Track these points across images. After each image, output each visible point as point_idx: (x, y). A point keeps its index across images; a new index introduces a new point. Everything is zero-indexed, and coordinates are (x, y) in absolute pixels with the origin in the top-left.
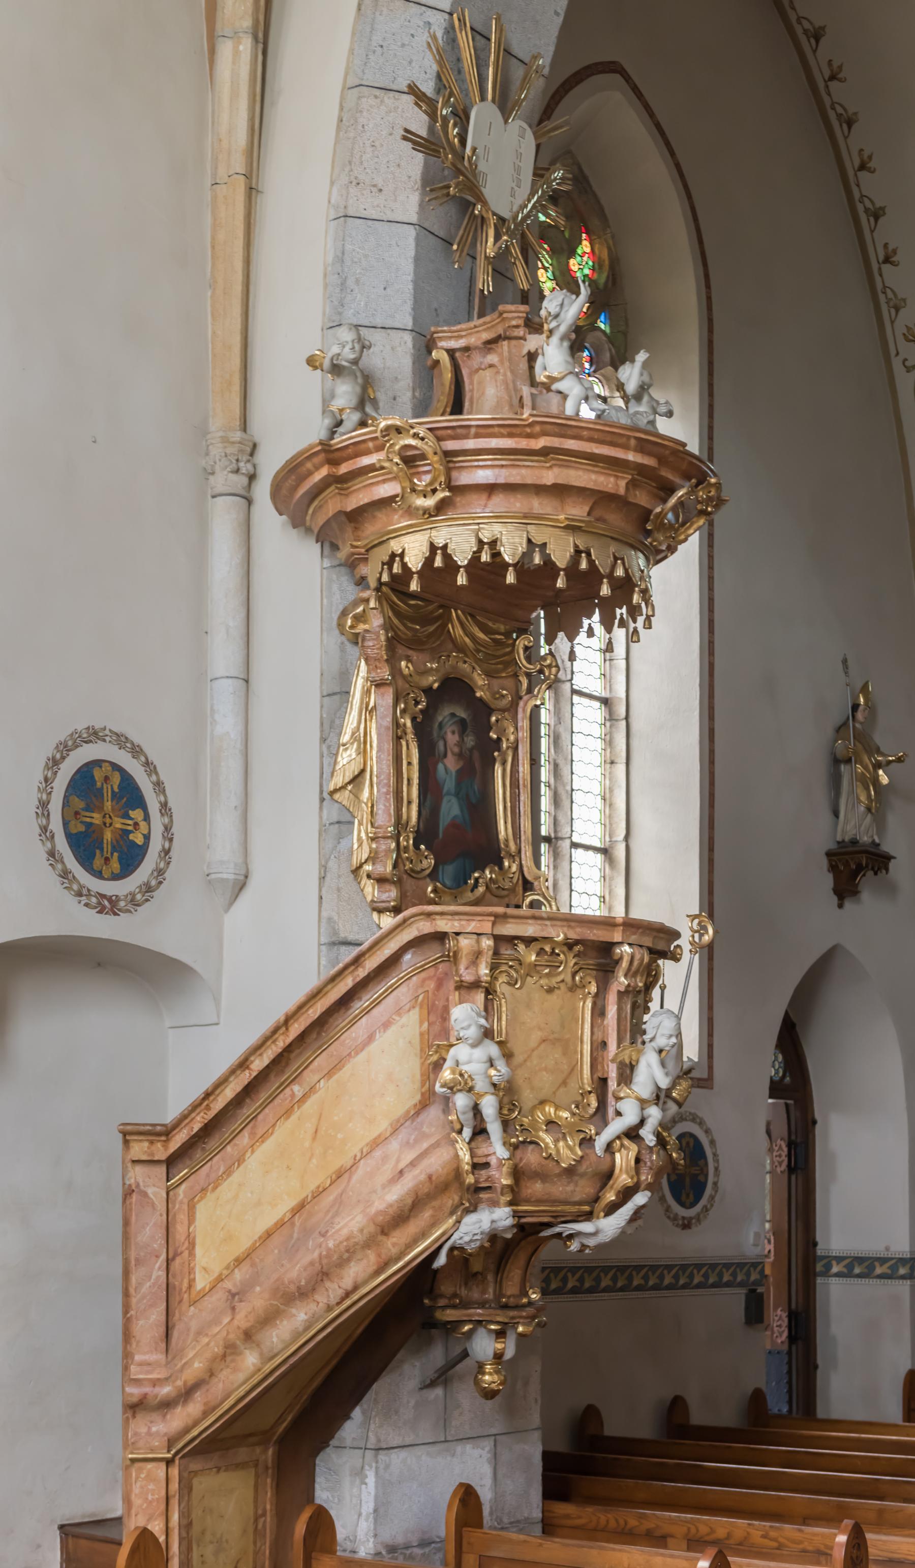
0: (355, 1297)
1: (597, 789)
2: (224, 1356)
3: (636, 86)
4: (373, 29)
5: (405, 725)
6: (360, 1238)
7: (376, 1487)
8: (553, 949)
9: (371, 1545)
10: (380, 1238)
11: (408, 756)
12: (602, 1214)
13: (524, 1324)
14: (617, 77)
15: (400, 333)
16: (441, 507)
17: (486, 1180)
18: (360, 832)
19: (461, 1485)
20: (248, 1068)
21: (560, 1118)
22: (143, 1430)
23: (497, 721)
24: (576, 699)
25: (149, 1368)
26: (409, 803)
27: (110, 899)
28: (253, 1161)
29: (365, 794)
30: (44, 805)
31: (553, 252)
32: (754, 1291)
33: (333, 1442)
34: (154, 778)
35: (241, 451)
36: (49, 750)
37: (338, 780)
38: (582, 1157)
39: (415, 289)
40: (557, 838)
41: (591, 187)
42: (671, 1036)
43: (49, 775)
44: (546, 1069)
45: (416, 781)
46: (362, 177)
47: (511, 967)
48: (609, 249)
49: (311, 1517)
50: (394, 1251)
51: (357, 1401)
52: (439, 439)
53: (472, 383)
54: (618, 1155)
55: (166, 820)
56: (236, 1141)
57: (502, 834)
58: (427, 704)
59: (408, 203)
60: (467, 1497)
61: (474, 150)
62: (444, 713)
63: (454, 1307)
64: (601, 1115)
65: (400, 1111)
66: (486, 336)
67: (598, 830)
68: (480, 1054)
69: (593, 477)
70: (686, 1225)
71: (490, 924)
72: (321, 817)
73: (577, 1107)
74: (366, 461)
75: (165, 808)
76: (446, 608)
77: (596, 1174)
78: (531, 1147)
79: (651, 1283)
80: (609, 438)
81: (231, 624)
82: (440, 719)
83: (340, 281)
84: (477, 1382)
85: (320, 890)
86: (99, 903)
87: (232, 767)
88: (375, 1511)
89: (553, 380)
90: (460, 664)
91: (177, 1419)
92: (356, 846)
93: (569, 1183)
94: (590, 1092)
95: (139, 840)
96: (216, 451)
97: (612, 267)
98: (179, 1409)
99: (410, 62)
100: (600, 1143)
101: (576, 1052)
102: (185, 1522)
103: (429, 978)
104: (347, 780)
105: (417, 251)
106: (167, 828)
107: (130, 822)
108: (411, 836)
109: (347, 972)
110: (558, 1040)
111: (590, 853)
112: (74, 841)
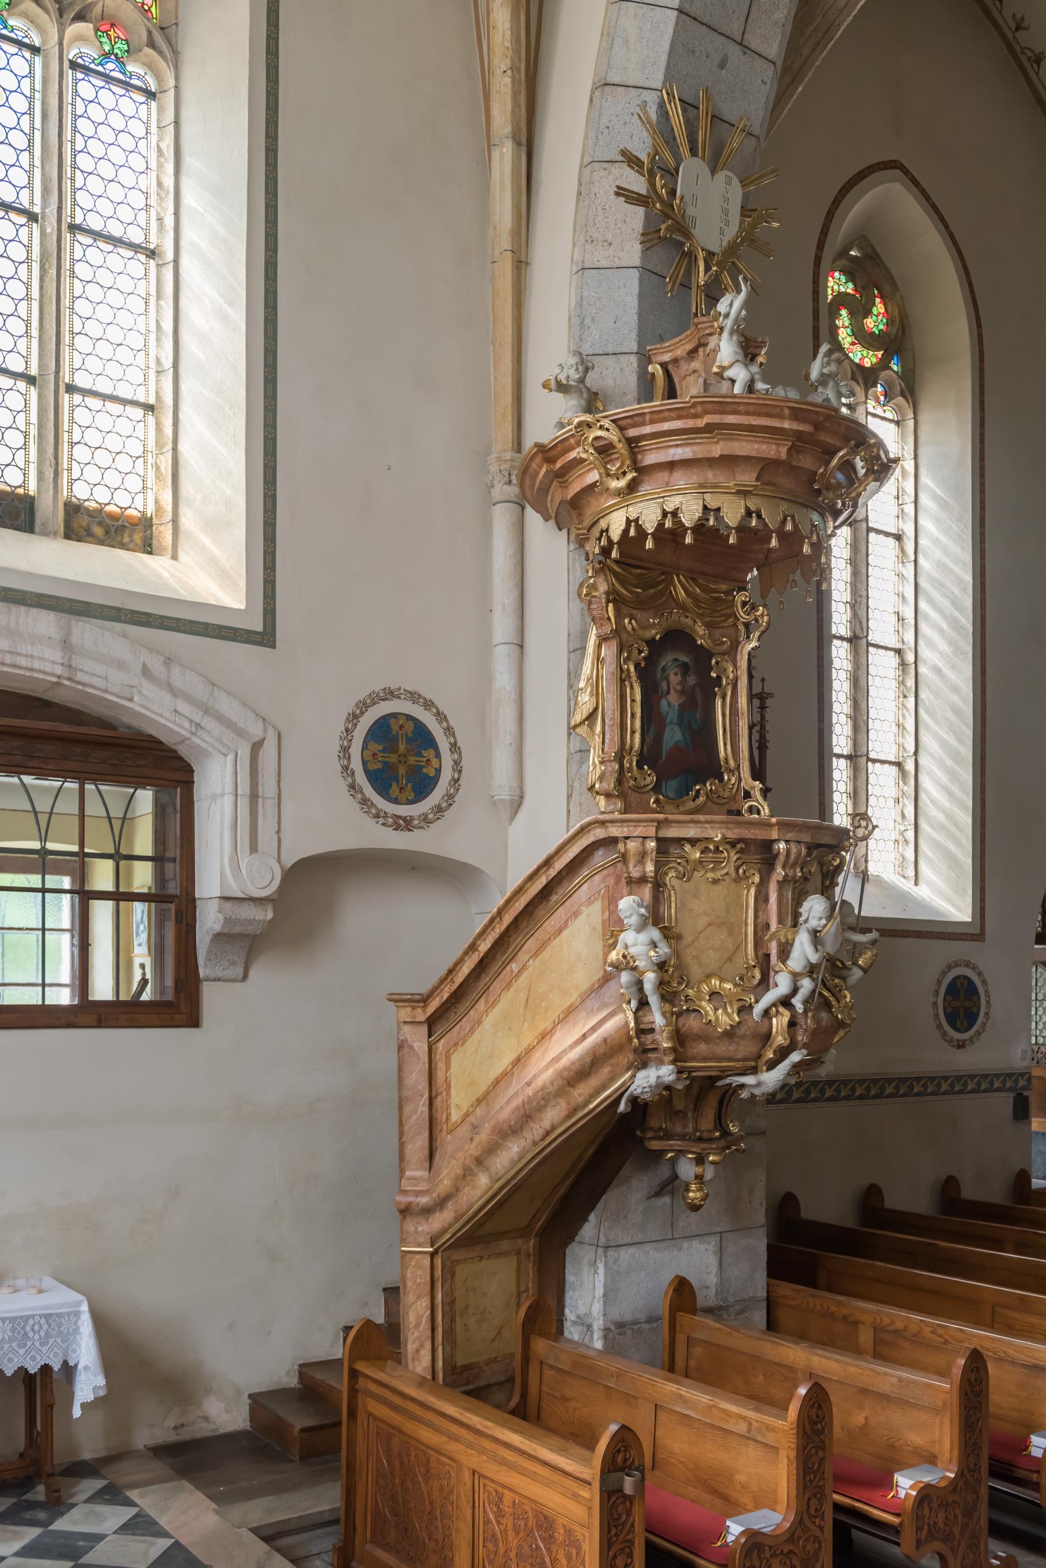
0: (553, 1136)
1: (892, 718)
2: (464, 1177)
3: (913, 177)
4: (600, 114)
5: (628, 670)
6: (552, 1089)
7: (605, 1277)
8: (717, 848)
9: (601, 1322)
10: (568, 1089)
11: (632, 694)
12: (765, 1068)
13: (714, 1154)
14: (897, 173)
15: (628, 357)
16: (632, 487)
17: (652, 1043)
18: (594, 757)
19: (677, 1276)
20: (476, 950)
21: (724, 989)
22: (412, 1229)
23: (717, 663)
24: (871, 649)
25: (415, 1182)
26: (633, 732)
27: (404, 819)
28: (488, 1022)
29: (598, 728)
30: (345, 750)
31: (851, 314)
32: (1021, 1094)
33: (577, 1238)
34: (445, 724)
35: (513, 467)
36: (350, 707)
37: (578, 718)
38: (739, 1023)
39: (639, 319)
40: (856, 756)
41: (882, 261)
42: (820, 919)
43: (350, 726)
44: (712, 948)
45: (639, 715)
46: (595, 235)
47: (679, 864)
48: (899, 307)
49: (529, 1307)
50: (580, 1100)
51: (592, 1208)
52: (622, 429)
53: (681, 389)
54: (774, 1020)
55: (456, 756)
56: (476, 1007)
57: (722, 754)
58: (650, 652)
59: (633, 253)
60: (682, 1288)
61: (682, 198)
62: (667, 659)
63: (660, 1138)
64: (765, 983)
65: (585, 986)
66: (689, 347)
67: (894, 749)
68: (643, 937)
69: (756, 446)
70: (961, 1045)
71: (654, 829)
72: (568, 747)
73: (741, 979)
74: (573, 455)
75: (454, 747)
76: (668, 575)
77: (755, 1036)
78: (694, 1014)
79: (929, 1090)
80: (764, 410)
81: (506, 602)
82: (664, 663)
83: (581, 321)
84: (685, 1198)
85: (568, 805)
86: (395, 822)
87: (506, 716)
88: (604, 1296)
89: (723, 369)
90: (683, 619)
91: (439, 1221)
92: (591, 768)
93: (730, 1044)
94: (754, 967)
95: (432, 773)
96: (494, 468)
97: (901, 321)
98: (437, 1214)
99: (632, 137)
100: (758, 1009)
101: (741, 933)
102: (448, 1300)
103: (609, 875)
104: (584, 717)
105: (640, 289)
106: (457, 763)
107: (381, 759)
108: (635, 759)
109: (541, 872)
110: (724, 923)
111: (887, 765)
112: (373, 777)
